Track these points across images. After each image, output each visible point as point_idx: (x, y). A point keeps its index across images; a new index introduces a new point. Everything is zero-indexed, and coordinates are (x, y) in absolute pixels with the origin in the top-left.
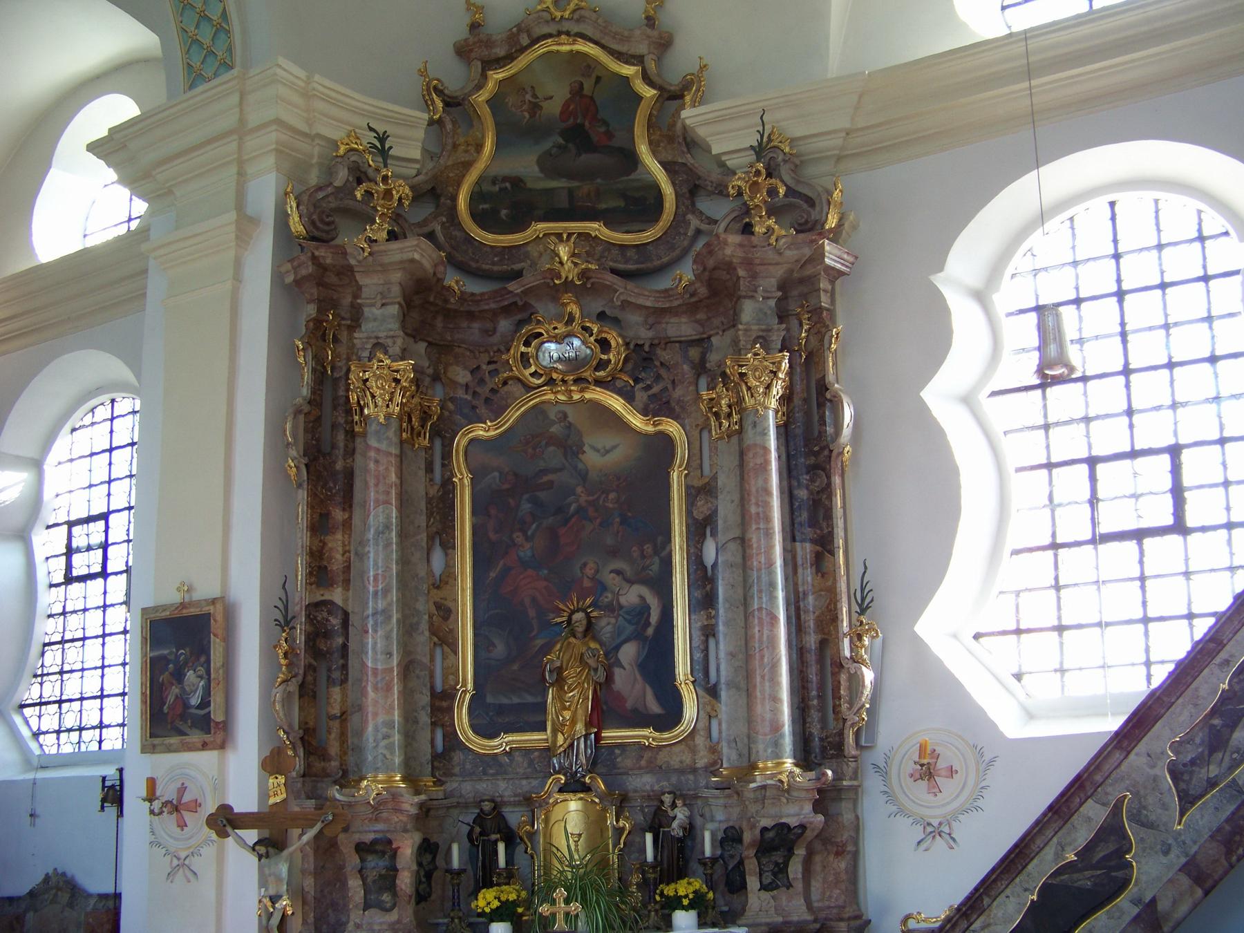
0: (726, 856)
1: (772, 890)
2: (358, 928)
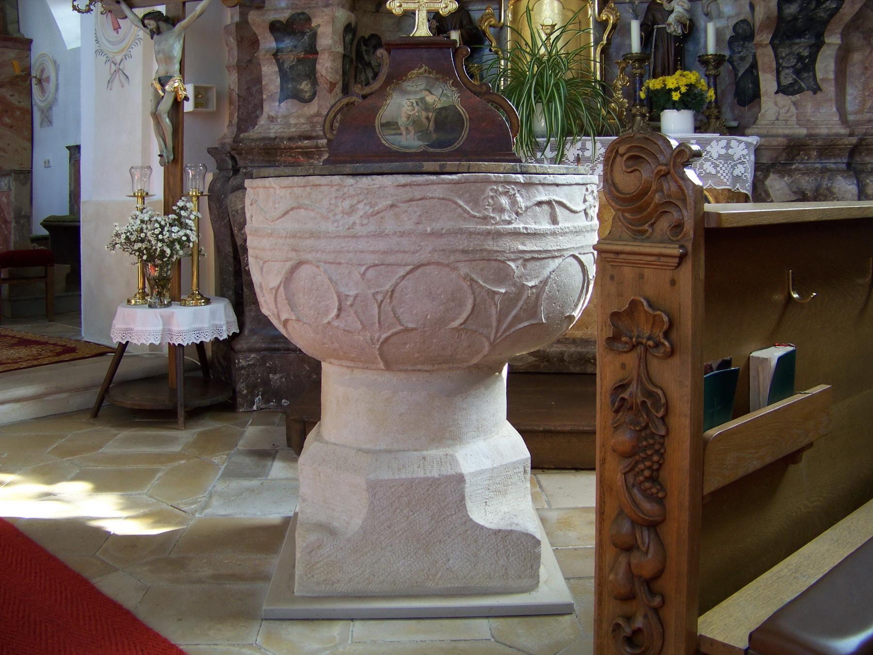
0: (735, 58)
1: (793, 93)
2: (272, 121)
